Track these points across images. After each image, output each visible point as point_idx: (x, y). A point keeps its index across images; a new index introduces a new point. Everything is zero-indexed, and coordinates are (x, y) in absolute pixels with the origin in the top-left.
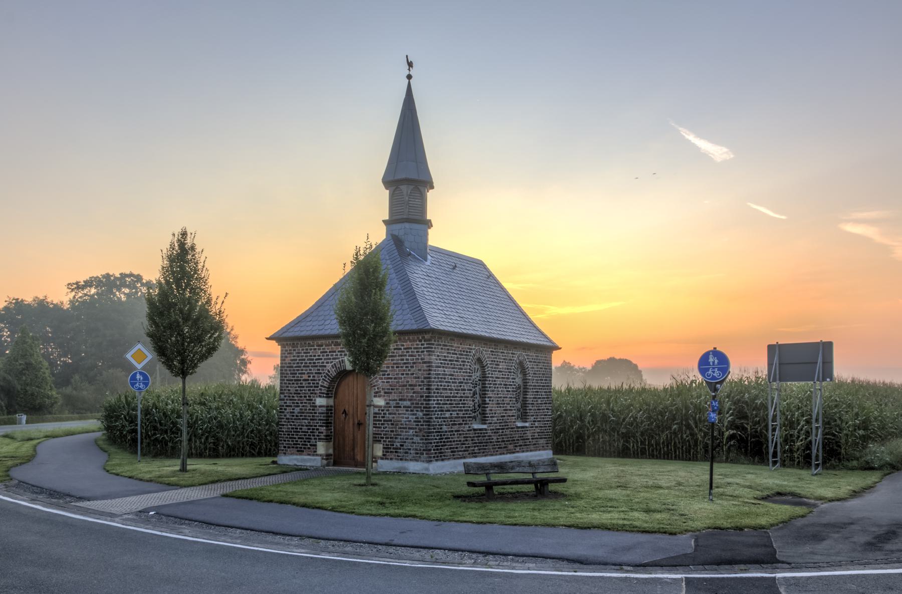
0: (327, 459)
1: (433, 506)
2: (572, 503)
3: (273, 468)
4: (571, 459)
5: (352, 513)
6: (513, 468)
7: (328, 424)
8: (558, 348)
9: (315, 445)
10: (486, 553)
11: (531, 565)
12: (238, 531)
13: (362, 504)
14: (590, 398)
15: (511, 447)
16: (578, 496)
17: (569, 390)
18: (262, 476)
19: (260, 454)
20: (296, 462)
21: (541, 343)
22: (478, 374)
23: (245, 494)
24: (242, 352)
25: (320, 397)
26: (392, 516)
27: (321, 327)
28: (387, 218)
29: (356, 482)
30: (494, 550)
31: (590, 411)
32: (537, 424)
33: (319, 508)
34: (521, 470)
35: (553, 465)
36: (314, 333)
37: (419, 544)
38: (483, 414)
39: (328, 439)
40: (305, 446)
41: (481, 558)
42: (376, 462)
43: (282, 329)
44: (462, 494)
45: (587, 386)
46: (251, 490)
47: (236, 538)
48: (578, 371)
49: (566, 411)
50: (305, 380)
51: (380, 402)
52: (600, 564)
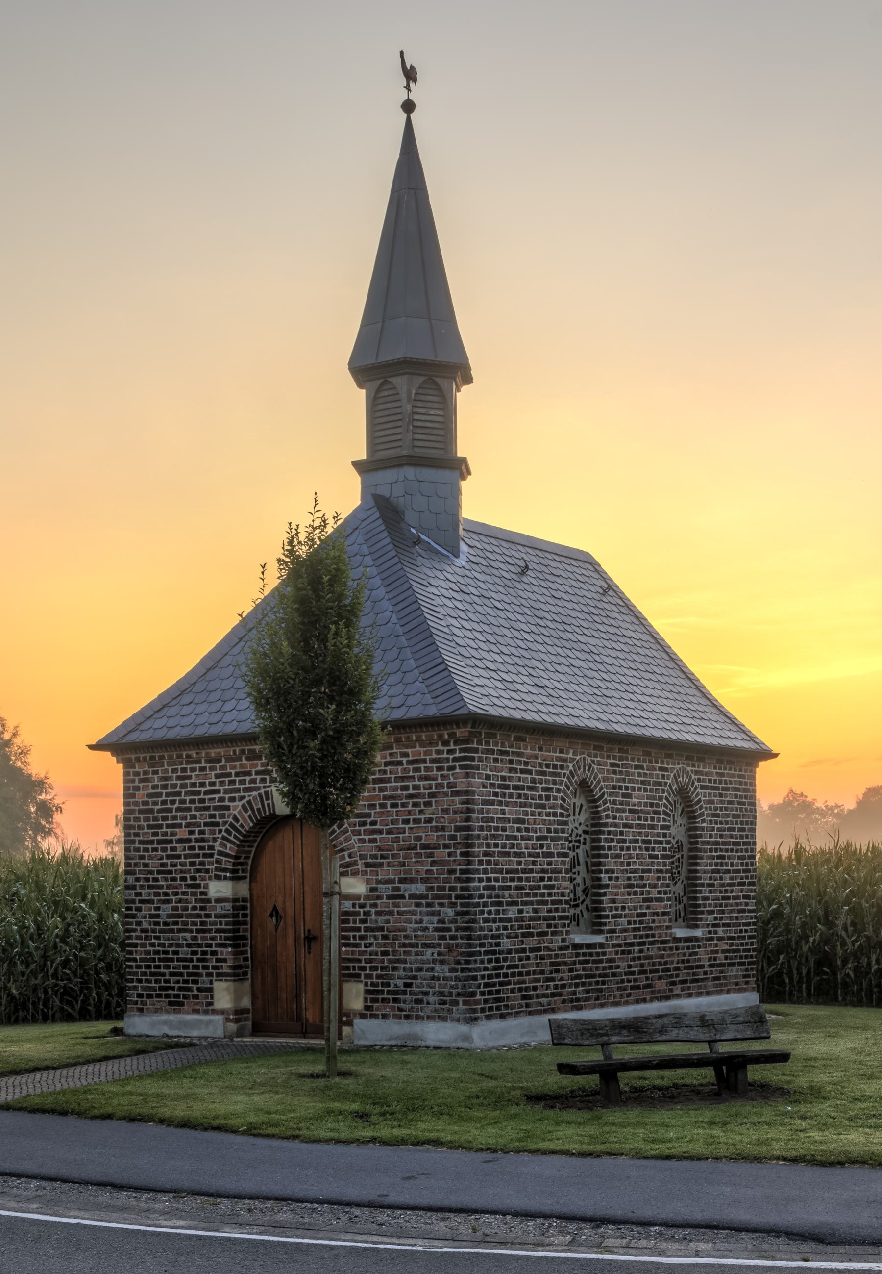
0: (237, 1021)
1: (479, 1120)
2: (803, 1108)
3: (114, 1044)
4: (802, 1012)
5: (295, 1137)
6: (663, 1030)
7: (236, 941)
8: (769, 755)
9: (210, 990)
10: (598, 1221)
11: (702, 1246)
12: (34, 1183)
13: (318, 1118)
14: (848, 871)
15: (661, 985)
16: (816, 1093)
17: (798, 852)
18: (88, 1062)
19: (84, 1016)
20: (166, 1030)
21: (731, 743)
22: (582, 818)
23: (49, 1102)
24: (40, 785)
25: (218, 878)
26: (384, 1143)
27: (215, 718)
28: (362, 455)
29: (303, 1069)
30: (617, 1212)
31: (847, 902)
32: (721, 931)
33: (218, 1129)
34: (682, 1034)
35: (757, 1023)
36: (200, 732)
37: (446, 1203)
38: (596, 909)
39: (237, 974)
40: (183, 993)
41: (587, 1232)
42: (350, 1024)
43: (125, 723)
44: (546, 1091)
45: (842, 842)
46: (63, 1092)
47: (29, 1200)
48: (823, 814)
49: (790, 902)
50: (180, 841)
51: (355, 886)
52: (863, 1242)
